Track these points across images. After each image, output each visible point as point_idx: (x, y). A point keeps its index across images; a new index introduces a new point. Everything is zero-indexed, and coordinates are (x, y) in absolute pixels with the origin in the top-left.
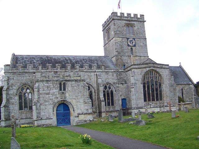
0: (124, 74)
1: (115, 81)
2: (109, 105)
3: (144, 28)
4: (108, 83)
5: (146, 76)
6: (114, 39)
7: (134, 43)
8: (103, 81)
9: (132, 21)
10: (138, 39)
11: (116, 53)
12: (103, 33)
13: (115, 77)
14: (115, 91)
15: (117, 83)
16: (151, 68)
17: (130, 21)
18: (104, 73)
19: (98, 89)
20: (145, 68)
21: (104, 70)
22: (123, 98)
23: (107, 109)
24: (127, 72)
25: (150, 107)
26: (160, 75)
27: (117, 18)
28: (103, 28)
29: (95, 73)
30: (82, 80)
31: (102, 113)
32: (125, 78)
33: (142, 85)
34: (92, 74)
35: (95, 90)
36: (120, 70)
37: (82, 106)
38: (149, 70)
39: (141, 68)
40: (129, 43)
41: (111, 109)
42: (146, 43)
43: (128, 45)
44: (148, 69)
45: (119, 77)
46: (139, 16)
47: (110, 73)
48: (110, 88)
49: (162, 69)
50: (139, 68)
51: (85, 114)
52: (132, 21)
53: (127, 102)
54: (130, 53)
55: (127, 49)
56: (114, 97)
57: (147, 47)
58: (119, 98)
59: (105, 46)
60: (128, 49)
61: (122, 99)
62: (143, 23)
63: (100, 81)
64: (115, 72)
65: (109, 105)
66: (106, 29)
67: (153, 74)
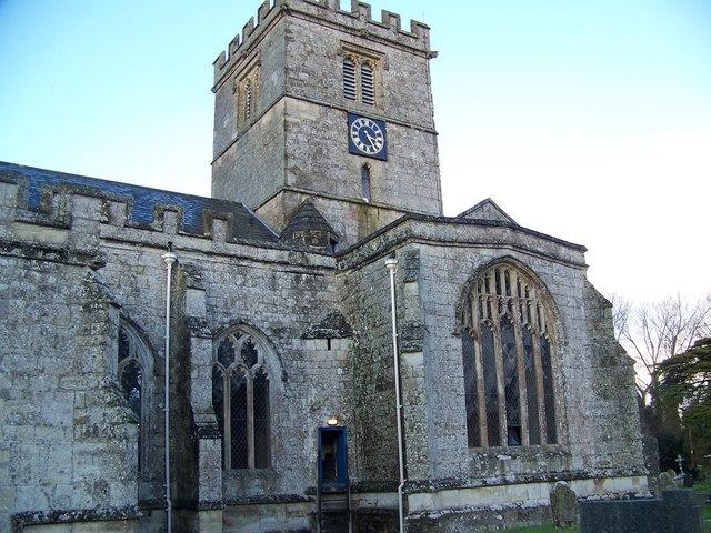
1: (287, 320)
2: (245, 464)
4: (239, 324)
13: (285, 293)
14: (284, 380)
16: (505, 252)
19: (183, 357)
20: (474, 244)
21: (221, 246)
23: (233, 491)
26: (548, 297)
30: (82, 255)
33: (458, 343)
35: (159, 362)
38: (493, 262)
39: (451, 243)
40: (357, 140)
41: (256, 488)
42: (436, 153)
43: (353, 150)
44: (488, 254)
45: (308, 295)
46: (406, 27)
47: (259, 270)
48: (250, 353)
49: (556, 266)
50: (443, 242)
54: (358, 187)
56: (274, 417)
57: (437, 173)
59: (220, 161)
60: (348, 167)
62: (422, 60)
64: (286, 264)
65: (494, 439)
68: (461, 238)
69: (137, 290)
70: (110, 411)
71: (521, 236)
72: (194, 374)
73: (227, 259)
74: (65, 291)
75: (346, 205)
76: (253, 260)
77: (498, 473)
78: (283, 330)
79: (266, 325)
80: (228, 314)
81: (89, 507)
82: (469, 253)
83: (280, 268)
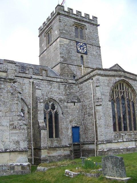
0: (75, 88)
1: (63, 98)
2: (52, 137)
3: (98, 33)
4: (51, 99)
5: (115, 90)
6: (58, 40)
7: (85, 50)
8: (43, 95)
9: (83, 21)
10: (91, 46)
11: (59, 60)
12: (40, 39)
13: (62, 90)
15: (64, 101)
16: (122, 78)
17: (80, 21)
18: (45, 83)
19: (35, 108)
21: (45, 78)
22: (74, 125)
24: (81, 83)
25: (122, 141)
27: (64, 14)
28: (39, 32)
29: (31, 80)
30: (11, 79)
31: (42, 151)
32: (78, 94)
33: (110, 103)
34: (26, 81)
35: (29, 109)
36: (70, 81)
37: (7, 134)
38: (119, 81)
41: (55, 144)
42: (100, 52)
44: (117, 79)
45: (68, 91)
47: (55, 84)
51: (13, 152)
52: (83, 21)
53: (81, 133)
55: (75, 57)
56: (60, 124)
57: (101, 57)
58: (67, 125)
59: (41, 56)
61: (73, 127)
62: (96, 27)
63: (38, 93)
66: (46, 31)
67: (124, 88)
68: (110, 74)
69: (23, 90)
70: (19, 122)
71: (126, 74)
72: (39, 112)
73: (47, 81)
74: (6, 89)
75: (77, 67)
76: (53, 81)
77: (121, 138)
78: (62, 100)
79: (57, 99)
80: (47, 96)
81: (15, 148)
82: (113, 78)
83: (61, 83)
